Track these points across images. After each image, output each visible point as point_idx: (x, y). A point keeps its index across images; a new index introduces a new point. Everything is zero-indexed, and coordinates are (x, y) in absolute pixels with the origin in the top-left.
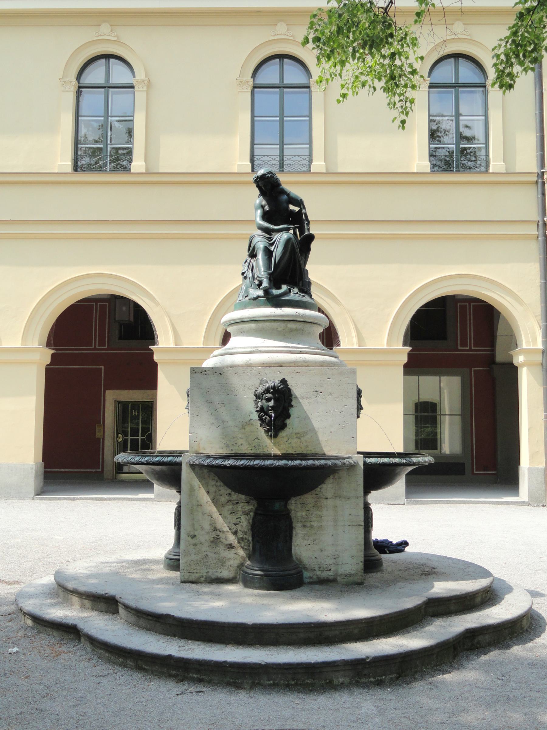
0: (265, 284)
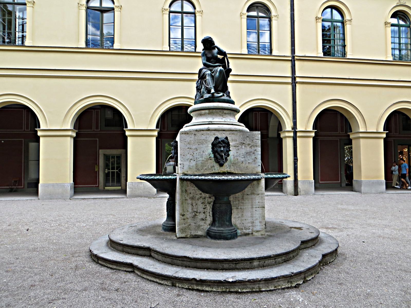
0: (213, 91)
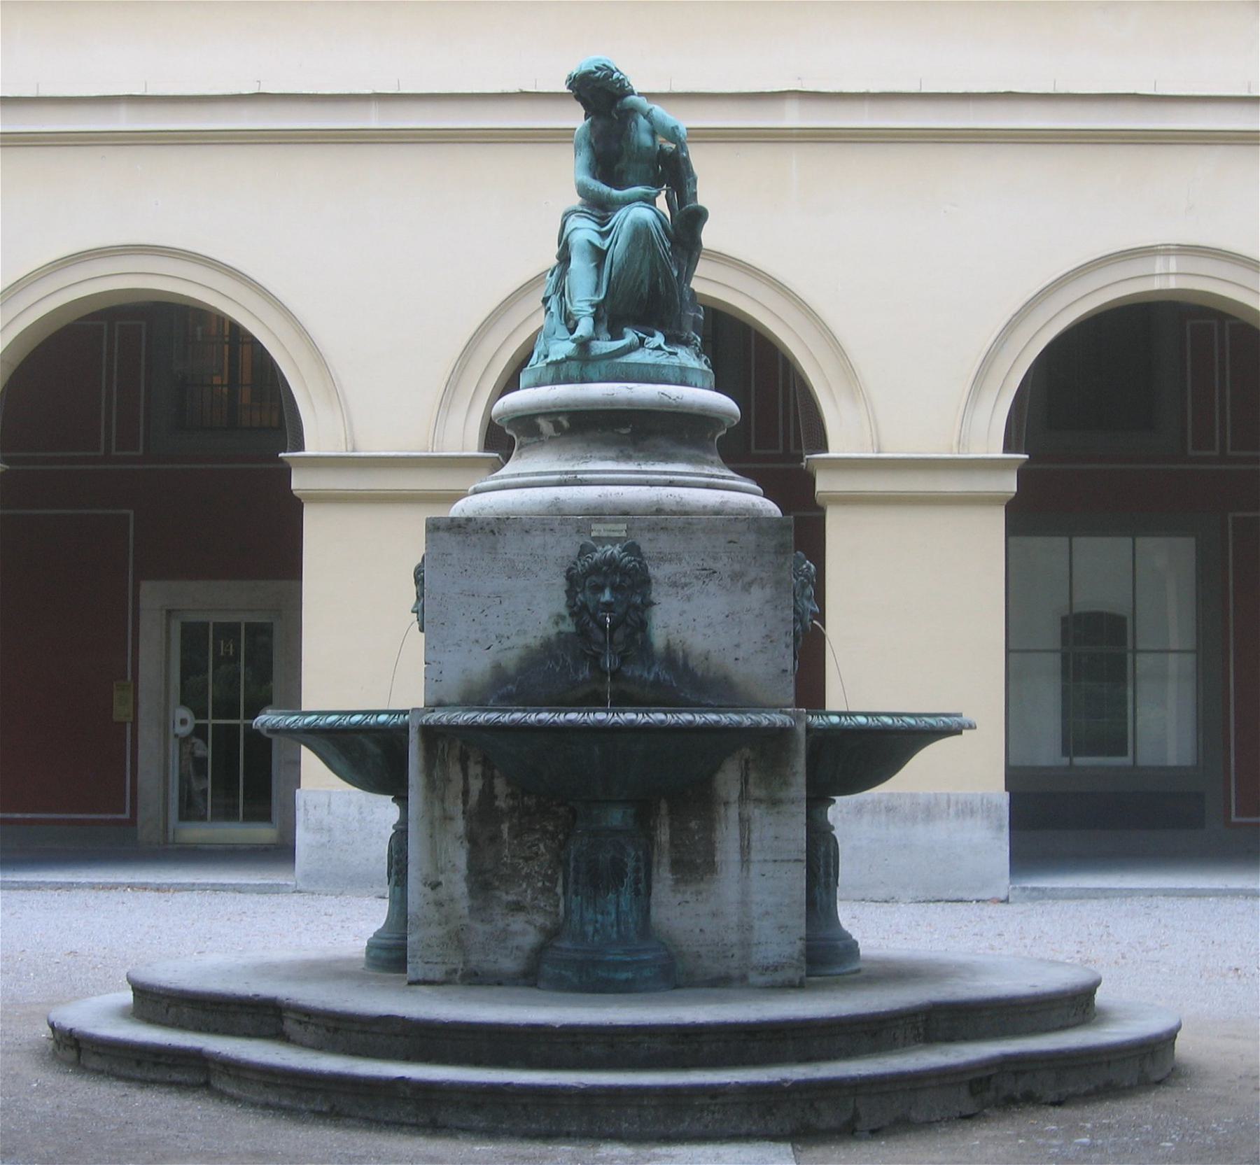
0: (585, 327)
